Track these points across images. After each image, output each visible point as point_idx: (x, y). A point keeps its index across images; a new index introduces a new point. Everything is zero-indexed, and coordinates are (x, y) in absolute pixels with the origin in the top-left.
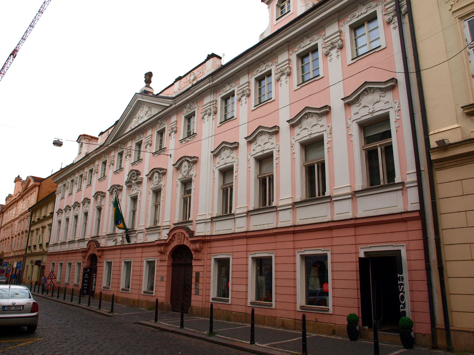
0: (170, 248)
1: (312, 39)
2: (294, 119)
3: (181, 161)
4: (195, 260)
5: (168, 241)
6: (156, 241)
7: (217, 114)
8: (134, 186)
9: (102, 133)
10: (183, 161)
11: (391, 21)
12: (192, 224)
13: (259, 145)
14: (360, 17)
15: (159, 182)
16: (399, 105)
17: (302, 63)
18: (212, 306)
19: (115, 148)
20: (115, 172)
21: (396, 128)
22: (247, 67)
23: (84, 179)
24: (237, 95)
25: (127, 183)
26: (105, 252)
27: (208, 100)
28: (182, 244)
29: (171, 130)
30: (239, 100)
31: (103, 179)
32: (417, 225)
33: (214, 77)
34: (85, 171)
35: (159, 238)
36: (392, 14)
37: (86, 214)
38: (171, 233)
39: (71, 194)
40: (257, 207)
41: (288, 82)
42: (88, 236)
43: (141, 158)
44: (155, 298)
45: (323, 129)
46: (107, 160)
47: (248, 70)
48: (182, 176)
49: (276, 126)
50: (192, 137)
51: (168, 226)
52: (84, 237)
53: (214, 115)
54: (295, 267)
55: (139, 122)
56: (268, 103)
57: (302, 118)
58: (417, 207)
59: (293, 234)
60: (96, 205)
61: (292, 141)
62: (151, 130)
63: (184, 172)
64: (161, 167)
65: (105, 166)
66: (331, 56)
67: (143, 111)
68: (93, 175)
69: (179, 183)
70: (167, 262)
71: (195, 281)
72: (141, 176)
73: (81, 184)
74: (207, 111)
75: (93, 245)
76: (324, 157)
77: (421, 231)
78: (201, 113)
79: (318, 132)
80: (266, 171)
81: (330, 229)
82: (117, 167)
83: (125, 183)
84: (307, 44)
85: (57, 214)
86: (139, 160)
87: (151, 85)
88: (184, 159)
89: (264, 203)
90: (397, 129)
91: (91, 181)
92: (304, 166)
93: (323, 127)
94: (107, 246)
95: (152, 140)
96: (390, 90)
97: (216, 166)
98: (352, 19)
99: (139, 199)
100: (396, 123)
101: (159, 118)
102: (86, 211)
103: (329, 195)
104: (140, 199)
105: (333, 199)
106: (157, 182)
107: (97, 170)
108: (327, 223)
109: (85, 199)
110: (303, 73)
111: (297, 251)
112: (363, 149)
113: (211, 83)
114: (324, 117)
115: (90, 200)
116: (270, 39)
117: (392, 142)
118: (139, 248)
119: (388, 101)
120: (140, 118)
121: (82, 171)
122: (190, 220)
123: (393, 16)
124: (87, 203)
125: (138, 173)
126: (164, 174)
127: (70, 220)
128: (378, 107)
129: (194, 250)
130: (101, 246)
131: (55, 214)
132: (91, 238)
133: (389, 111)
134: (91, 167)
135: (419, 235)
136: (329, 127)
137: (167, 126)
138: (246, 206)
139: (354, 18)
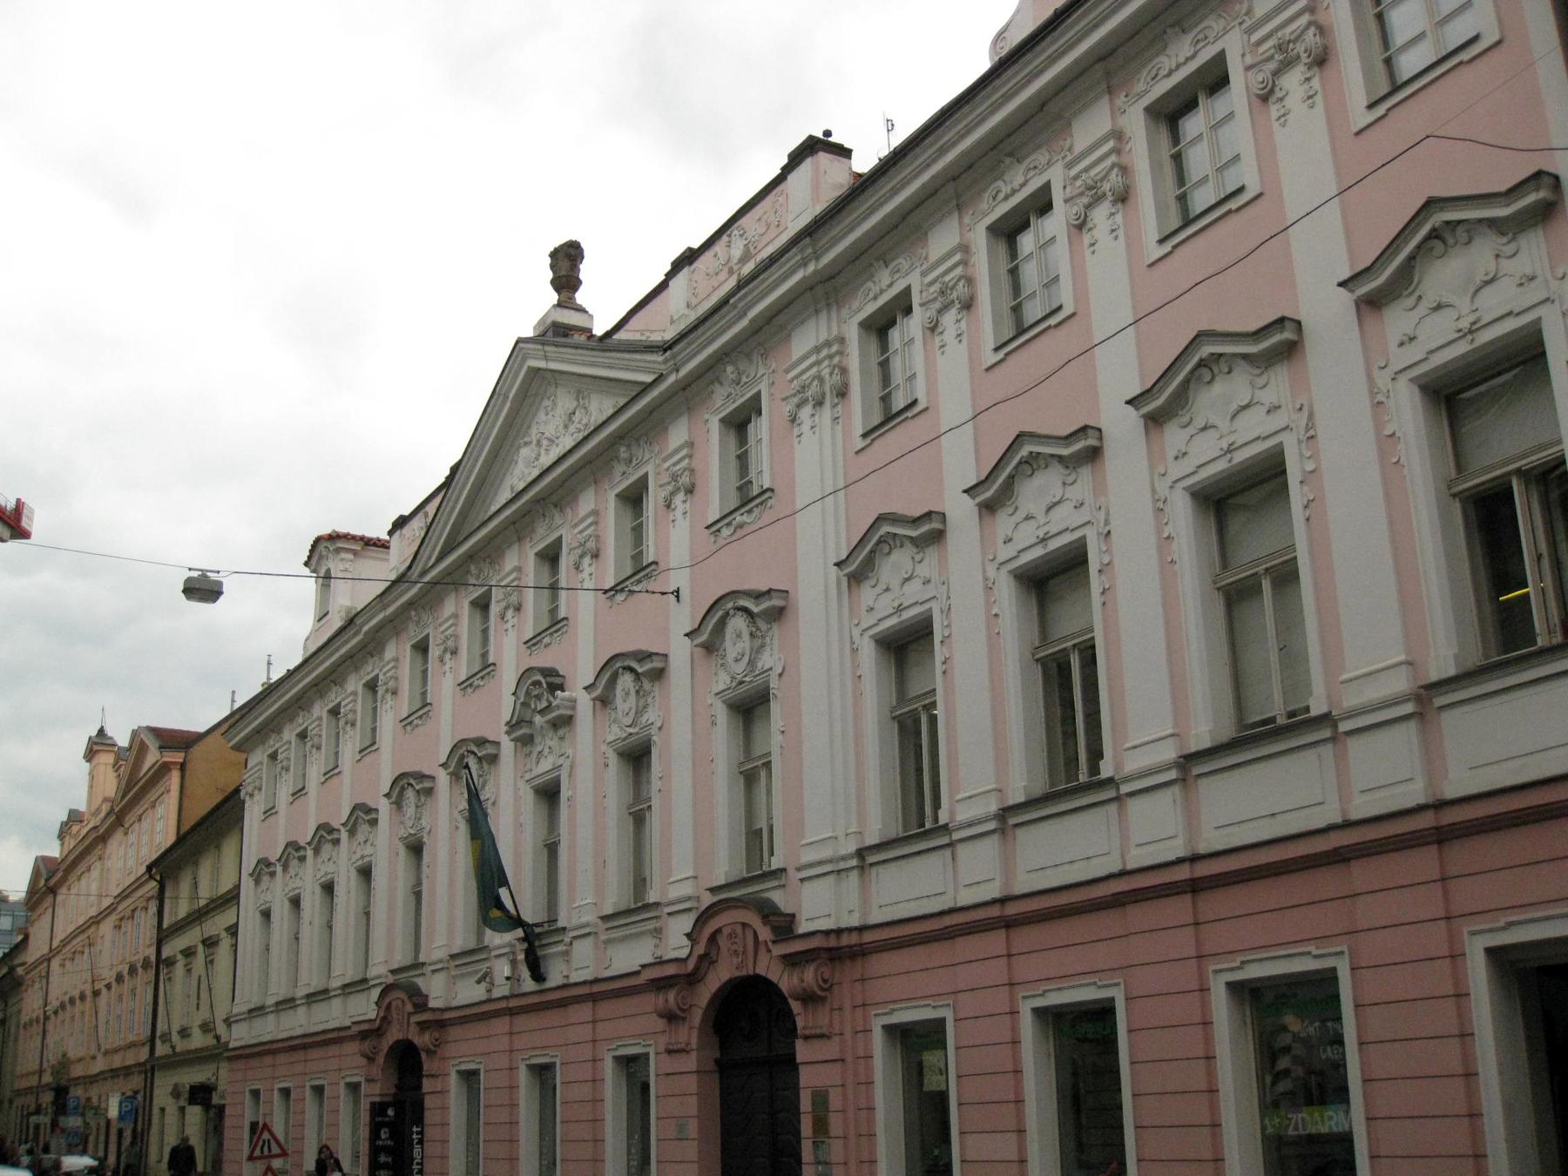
3: (720, 613)
5: (691, 965)
6: (644, 966)
10: (728, 613)
12: (782, 883)
13: (1028, 518)
19: (452, 581)
20: (466, 685)
25: (512, 726)
26: (874, 958)
27: (806, 339)
28: (751, 973)
29: (669, 483)
30: (933, 328)
31: (421, 717)
34: (349, 691)
35: (659, 953)
37: (366, 873)
40: (1039, 789)
42: (379, 970)
45: (1279, 420)
51: (689, 898)
55: (541, 461)
56: (1051, 332)
60: (403, 833)
61: (1156, 485)
63: (737, 660)
68: (379, 704)
69: (721, 713)
71: (814, 1133)
72: (566, 694)
76: (1292, 547)
78: (783, 400)
79: (1067, 529)
83: (505, 728)
84: (1182, 59)
85: (252, 883)
86: (556, 623)
87: (581, 297)
88: (730, 605)
91: (374, 730)
93: (1279, 411)
94: (455, 1003)
96: (1535, 225)
97: (865, 626)
99: (565, 793)
103: (1324, 709)
104: (570, 793)
105: (1344, 727)
106: (633, 711)
111: (1212, 968)
112: (1454, 496)
113: (811, 268)
115: (377, 810)
120: (545, 442)
121: (334, 689)
125: (553, 681)
126: (659, 675)
128: (1493, 302)
131: (247, 884)
133: (1084, 537)
136: (1301, 409)
137: (655, 466)
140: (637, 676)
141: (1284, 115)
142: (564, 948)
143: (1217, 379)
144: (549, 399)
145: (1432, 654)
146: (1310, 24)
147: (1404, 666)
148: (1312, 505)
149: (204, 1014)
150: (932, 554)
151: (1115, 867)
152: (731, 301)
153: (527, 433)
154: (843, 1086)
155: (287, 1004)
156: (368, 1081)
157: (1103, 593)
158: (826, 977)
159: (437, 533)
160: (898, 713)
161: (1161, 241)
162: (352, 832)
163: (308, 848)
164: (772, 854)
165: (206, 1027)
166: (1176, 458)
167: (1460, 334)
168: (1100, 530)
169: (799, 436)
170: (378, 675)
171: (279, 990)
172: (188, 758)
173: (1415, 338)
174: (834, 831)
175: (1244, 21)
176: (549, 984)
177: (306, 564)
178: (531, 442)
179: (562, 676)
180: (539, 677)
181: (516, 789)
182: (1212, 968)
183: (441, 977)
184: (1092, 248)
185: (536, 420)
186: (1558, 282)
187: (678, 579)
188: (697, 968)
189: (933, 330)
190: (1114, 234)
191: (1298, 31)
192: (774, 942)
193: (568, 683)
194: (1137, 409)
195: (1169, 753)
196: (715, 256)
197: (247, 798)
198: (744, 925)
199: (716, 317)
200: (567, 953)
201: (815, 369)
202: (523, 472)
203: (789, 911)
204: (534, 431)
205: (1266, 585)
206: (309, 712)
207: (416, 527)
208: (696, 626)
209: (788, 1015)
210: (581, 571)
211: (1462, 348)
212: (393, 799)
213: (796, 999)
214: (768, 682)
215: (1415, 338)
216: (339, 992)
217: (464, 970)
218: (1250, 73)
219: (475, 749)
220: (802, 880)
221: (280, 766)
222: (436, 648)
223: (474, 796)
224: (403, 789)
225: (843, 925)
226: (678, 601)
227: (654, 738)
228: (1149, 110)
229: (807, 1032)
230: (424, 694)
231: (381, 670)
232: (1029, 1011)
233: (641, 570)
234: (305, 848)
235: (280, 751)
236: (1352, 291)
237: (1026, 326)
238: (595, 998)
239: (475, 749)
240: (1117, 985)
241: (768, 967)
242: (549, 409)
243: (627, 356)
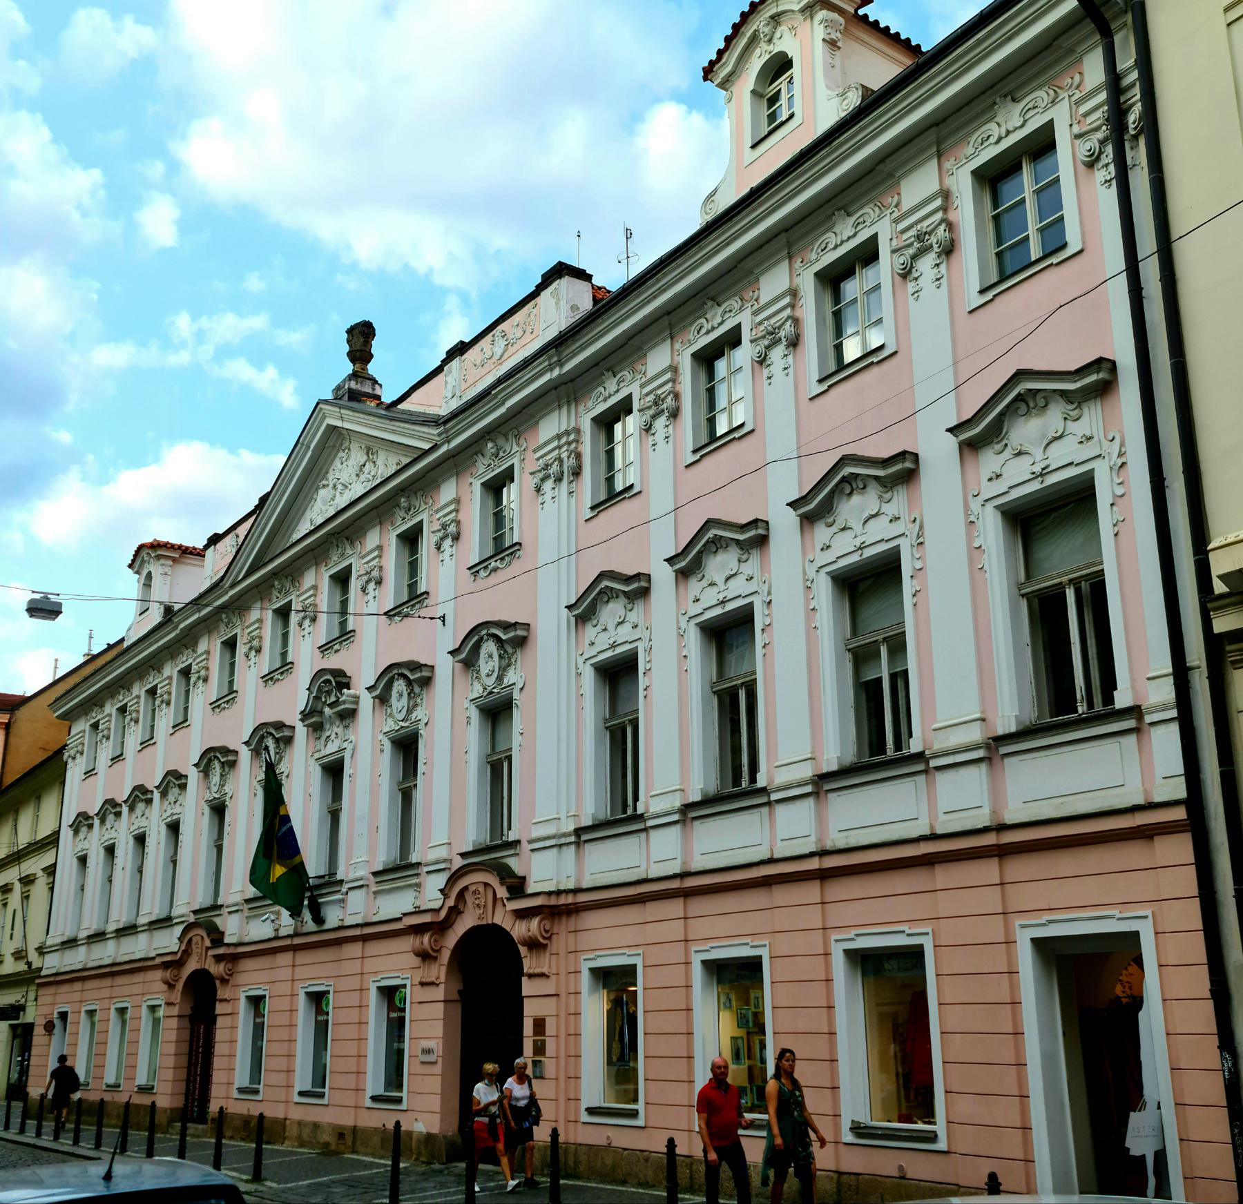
1: (861, 220)
2: (809, 497)
3: (476, 638)
4: (530, 976)
5: (443, 914)
6: (405, 915)
7: (580, 478)
8: (331, 724)
9: (215, 540)
10: (482, 638)
11: (1098, 158)
12: (518, 852)
13: (712, 584)
15: (409, 711)
17: (996, 204)
19: (261, 591)
20: (268, 678)
21: (1115, 525)
22: (666, 317)
23: (162, 702)
24: (752, 341)
25: (305, 715)
27: (550, 426)
28: (490, 922)
29: (439, 531)
30: (648, 429)
31: (228, 701)
32: (1180, 849)
33: (564, 350)
34: (165, 676)
35: (417, 904)
36: (1100, 135)
37: (174, 828)
38: (184, 937)
39: (117, 758)
40: (712, 789)
41: (791, 370)
42: (183, 908)
43: (422, 588)
45: (898, 528)
46: (236, 634)
47: (671, 326)
48: (481, 690)
49: (756, 521)
50: (507, 555)
51: (445, 861)
52: (170, 913)
53: (572, 481)
54: (1014, 987)
55: (336, 502)
57: (832, 492)
58: (1179, 790)
59: (818, 882)
60: (208, 796)
61: (807, 569)
62: (378, 528)
63: (488, 675)
64: (416, 659)
65: (233, 655)
67: (350, 463)
68: (191, 687)
69: (474, 714)
70: (442, 986)
71: (534, 1053)
72: (352, 692)
74: (551, 465)
75: (201, 938)
76: (754, 673)
77: (1194, 866)
78: (531, 474)
79: (1071, 464)
80: (737, 672)
82: (271, 662)
83: (300, 717)
84: (845, 238)
85: (71, 833)
86: (345, 635)
87: (373, 368)
89: (877, 745)
90: (1116, 529)
91: (186, 709)
92: (849, 650)
93: (898, 522)
95: (384, 563)
96: (1095, 397)
97: (586, 656)
98: (981, 148)
99: (347, 770)
100: (1115, 508)
101: (401, 490)
102: (142, 830)
103: (919, 749)
104: (351, 771)
105: (1148, 719)
106: (405, 709)
107: (203, 673)
109: (168, 773)
110: (999, 241)
111: (694, 948)
112: (1023, 596)
113: (556, 372)
114: (900, 488)
115: (186, 776)
116: (729, 224)
117: (1103, 570)
118: (286, 953)
119: (1088, 434)
120: (340, 487)
121: (152, 673)
122: (754, 787)
123: (1102, 142)
124: (176, 790)
125: (340, 680)
126: (427, 682)
127: (119, 852)
128: (1061, 453)
129: (525, 943)
130: (226, 940)
131: (66, 834)
132: (192, 914)
133: (751, 604)
134: (185, 659)
135: (1187, 880)
136: (914, 521)
137: (430, 518)
138: (678, 787)
139: (986, 144)
140: (409, 683)
141: (917, 292)
142: (341, 897)
143: (855, 492)
144: (344, 450)
145: (1000, 714)
146: (942, 221)
147: (979, 722)
148: (918, 594)
149: (17, 943)
150: (639, 606)
151: (766, 855)
152: (493, 393)
153: (325, 477)
154: (557, 1036)
155: (98, 937)
156: (169, 1004)
157: (764, 647)
160: (609, 724)
161: (821, 381)
162: (164, 795)
163: (95, 818)
164: (509, 828)
165: (19, 955)
166: (822, 549)
167: (1034, 476)
168: (764, 599)
169: (542, 504)
170: (190, 665)
171: (91, 924)
172: (12, 720)
173: (1001, 475)
174: (558, 813)
175: (893, 212)
176: (327, 926)
177: (130, 566)
178: (328, 485)
179: (350, 677)
180: (329, 677)
181: (307, 766)
182: (833, 937)
183: (235, 917)
184: (769, 381)
185: (333, 467)
186: (1109, 443)
187: (447, 609)
188: (181, 958)
189: (647, 430)
190: (786, 371)
192: (508, 899)
193: (354, 682)
194: (795, 510)
195: (806, 772)
196: (482, 350)
197: (70, 760)
198: (486, 885)
200: (342, 901)
201: (556, 452)
202: (321, 510)
203: (521, 874)
204: (331, 476)
205: (884, 651)
206: (129, 690)
207: (228, 545)
208: (457, 646)
210: (367, 594)
211: (1035, 486)
212: (201, 769)
213: (523, 945)
214: (512, 693)
215: (1001, 475)
216: (146, 928)
217: (255, 912)
218: (894, 256)
219: (273, 731)
220: (532, 850)
221: (101, 734)
222: (243, 646)
223: (270, 768)
224: (210, 760)
225: (562, 887)
226: (444, 625)
227: (420, 732)
228: (818, 275)
229: (531, 971)
230: (231, 683)
231: (194, 660)
232: (700, 962)
233: (415, 597)
234: (120, 805)
235: (101, 722)
236: (956, 436)
238: (365, 939)
239: (273, 731)
240: (765, 946)
241: (501, 918)
242: (344, 459)
243: (407, 426)
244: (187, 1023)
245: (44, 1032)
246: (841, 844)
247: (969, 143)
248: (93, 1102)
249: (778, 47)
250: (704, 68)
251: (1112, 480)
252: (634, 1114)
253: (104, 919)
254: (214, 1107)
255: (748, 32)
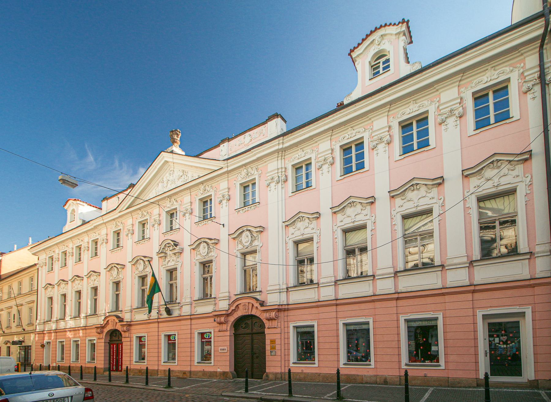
0: (232, 319)
3: (241, 231)
11: (375, 148)
14: (487, 83)
16: (531, 180)
18: (406, 372)
25: (158, 253)
28: (250, 314)
44: (146, 366)
45: (314, 231)
61: (392, 213)
66: (446, 125)
73: (52, 265)
78: (266, 180)
81: (443, 294)
85: (43, 290)
100: (526, 197)
105: (446, 268)
108: (529, 281)
139: (479, 84)
158: (277, 315)
159: (127, 201)
188: (104, 326)
191: (457, 108)
199: (245, 154)
209: (121, 334)
211: (494, 190)
237: (510, 117)
241: (119, 327)
244: (108, 344)
245: (41, 347)
246: (403, 291)
247: (473, 83)
248: (66, 367)
249: (382, 47)
250: (351, 50)
251: (526, 189)
252: (439, 366)
253: (63, 315)
254: (124, 367)
255: (370, 39)
